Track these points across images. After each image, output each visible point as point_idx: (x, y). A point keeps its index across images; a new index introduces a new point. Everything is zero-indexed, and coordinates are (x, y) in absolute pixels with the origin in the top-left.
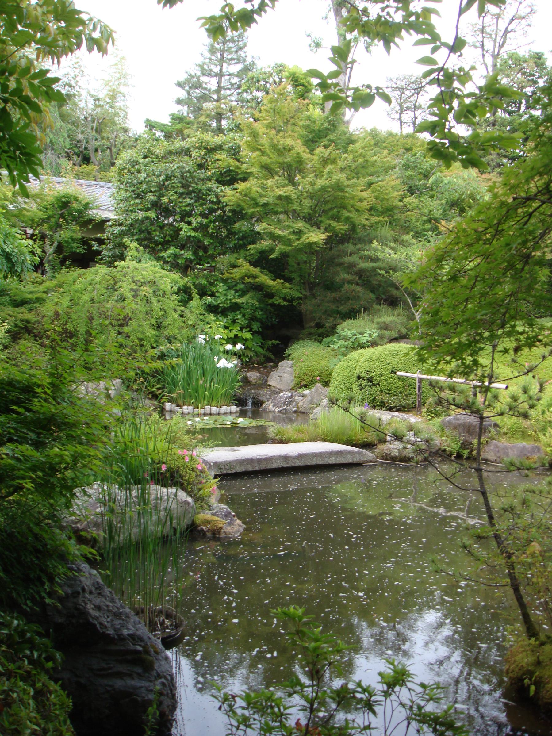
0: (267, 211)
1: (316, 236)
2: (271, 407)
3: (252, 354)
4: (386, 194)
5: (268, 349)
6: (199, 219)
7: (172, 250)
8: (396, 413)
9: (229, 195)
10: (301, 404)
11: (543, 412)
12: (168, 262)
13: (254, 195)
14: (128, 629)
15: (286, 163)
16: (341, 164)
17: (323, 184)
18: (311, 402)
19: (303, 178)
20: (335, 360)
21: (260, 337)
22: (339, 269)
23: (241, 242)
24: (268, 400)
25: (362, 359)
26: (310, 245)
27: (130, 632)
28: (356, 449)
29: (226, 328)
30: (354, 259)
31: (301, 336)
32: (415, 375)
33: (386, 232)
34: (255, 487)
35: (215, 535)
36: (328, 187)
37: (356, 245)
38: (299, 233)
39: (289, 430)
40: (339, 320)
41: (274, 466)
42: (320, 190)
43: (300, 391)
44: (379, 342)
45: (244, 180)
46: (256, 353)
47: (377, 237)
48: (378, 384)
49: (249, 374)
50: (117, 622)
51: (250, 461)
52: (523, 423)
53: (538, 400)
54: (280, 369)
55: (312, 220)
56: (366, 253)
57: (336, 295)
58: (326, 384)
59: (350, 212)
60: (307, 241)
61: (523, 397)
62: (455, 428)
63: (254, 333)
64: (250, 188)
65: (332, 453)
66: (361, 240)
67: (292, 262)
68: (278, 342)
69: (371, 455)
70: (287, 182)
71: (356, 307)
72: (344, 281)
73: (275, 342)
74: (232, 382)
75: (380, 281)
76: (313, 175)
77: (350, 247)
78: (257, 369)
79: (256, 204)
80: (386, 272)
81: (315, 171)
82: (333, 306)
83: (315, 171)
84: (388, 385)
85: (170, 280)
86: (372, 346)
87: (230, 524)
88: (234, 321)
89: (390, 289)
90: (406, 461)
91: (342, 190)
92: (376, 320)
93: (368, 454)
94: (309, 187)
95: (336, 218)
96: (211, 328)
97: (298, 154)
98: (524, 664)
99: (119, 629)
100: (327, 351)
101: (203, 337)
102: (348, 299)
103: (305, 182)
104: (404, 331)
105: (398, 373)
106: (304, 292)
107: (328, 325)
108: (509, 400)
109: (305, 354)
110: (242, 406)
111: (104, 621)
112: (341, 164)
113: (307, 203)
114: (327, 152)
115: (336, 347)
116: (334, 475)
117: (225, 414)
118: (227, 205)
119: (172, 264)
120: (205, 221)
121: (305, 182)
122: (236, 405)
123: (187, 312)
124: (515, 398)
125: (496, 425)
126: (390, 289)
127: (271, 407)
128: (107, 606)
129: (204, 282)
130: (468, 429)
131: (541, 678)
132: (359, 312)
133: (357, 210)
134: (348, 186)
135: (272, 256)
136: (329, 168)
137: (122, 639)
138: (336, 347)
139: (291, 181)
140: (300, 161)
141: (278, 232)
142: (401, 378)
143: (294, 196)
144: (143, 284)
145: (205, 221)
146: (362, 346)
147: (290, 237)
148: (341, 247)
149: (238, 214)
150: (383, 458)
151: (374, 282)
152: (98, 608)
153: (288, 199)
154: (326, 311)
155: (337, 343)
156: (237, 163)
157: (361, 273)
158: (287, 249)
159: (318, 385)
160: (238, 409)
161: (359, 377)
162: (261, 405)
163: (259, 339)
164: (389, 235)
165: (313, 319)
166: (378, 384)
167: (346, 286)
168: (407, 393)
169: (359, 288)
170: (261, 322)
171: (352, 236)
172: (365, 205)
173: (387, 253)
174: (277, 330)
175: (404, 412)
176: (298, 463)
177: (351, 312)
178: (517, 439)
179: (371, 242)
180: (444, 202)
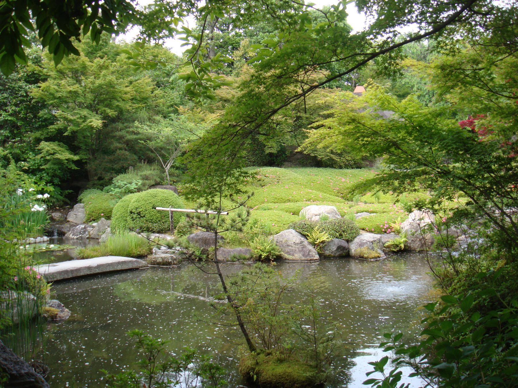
0: (61, 102)
1: (97, 122)
3: (54, 200)
4: (142, 88)
5: (66, 197)
8: (157, 235)
9: (35, 91)
10: (91, 232)
11: (251, 228)
14: (24, 370)
15: (75, 68)
16: (111, 69)
17: (100, 83)
18: (99, 231)
19: (86, 79)
20: (113, 201)
21: (59, 188)
22: (113, 140)
23: (44, 123)
25: (133, 200)
27: (26, 371)
28: (134, 259)
29: (35, 183)
30: (123, 133)
31: (88, 186)
32: (168, 209)
33: (144, 114)
34: (74, 288)
35: (53, 319)
37: (123, 123)
38: (85, 118)
39: (89, 249)
40: (114, 175)
41: (82, 274)
42: (98, 87)
43: (90, 224)
44: (142, 188)
45: (44, 80)
46: (57, 199)
49: (53, 214)
50: (17, 367)
51: (66, 272)
52: (240, 235)
53: (247, 221)
54: (75, 210)
56: (131, 130)
57: (111, 157)
58: (108, 218)
59: (118, 101)
61: (238, 220)
62: (197, 242)
65: (119, 263)
66: (127, 120)
67: (80, 136)
69: (144, 262)
70: (75, 82)
71: (125, 165)
72: (117, 148)
73: (70, 191)
74: (43, 221)
75: (141, 147)
76: (93, 77)
77: (120, 125)
78: (59, 210)
79: (55, 98)
80: (145, 141)
81: (94, 74)
83: (94, 74)
84: (151, 216)
87: (62, 311)
88: (41, 179)
89: (147, 152)
90: (167, 265)
91: (114, 87)
93: (142, 262)
95: (109, 106)
96: (25, 183)
97: (83, 62)
98: (250, 365)
99: (19, 371)
100: (107, 196)
101: (21, 190)
103: (88, 81)
104: (158, 180)
105: (157, 208)
106: (89, 156)
107: (107, 178)
108: (230, 221)
109: (92, 199)
110: (50, 236)
111: (9, 366)
112: (111, 69)
113: (90, 96)
114: (102, 61)
116: (117, 277)
117: (40, 242)
118: (33, 98)
120: (18, 109)
121: (88, 81)
122: (46, 236)
124: (234, 221)
125: (222, 238)
126: (147, 152)
127: (71, 236)
128: (10, 358)
129: (18, 151)
130: (205, 242)
131: (259, 371)
132: (128, 168)
133: (123, 100)
134: (117, 84)
135: (66, 134)
136: (104, 72)
137: (21, 375)
138: (113, 194)
139: (79, 81)
140: (84, 67)
141: (70, 117)
142: (159, 211)
143: (80, 92)
145: (18, 109)
146: (131, 192)
147: (79, 120)
148: (114, 125)
149: (42, 104)
150: (152, 264)
151: (137, 148)
152: (5, 359)
153: (75, 94)
154: (105, 168)
156: (40, 68)
158: (75, 129)
159: (103, 219)
160: (48, 239)
161: (131, 212)
164: (145, 116)
166: (144, 216)
168: (163, 221)
169: (127, 153)
171: (121, 117)
172: (128, 96)
173: (145, 129)
174: (70, 185)
175: (162, 233)
176: (97, 271)
178: (236, 245)
179: (134, 121)
180: (181, 93)
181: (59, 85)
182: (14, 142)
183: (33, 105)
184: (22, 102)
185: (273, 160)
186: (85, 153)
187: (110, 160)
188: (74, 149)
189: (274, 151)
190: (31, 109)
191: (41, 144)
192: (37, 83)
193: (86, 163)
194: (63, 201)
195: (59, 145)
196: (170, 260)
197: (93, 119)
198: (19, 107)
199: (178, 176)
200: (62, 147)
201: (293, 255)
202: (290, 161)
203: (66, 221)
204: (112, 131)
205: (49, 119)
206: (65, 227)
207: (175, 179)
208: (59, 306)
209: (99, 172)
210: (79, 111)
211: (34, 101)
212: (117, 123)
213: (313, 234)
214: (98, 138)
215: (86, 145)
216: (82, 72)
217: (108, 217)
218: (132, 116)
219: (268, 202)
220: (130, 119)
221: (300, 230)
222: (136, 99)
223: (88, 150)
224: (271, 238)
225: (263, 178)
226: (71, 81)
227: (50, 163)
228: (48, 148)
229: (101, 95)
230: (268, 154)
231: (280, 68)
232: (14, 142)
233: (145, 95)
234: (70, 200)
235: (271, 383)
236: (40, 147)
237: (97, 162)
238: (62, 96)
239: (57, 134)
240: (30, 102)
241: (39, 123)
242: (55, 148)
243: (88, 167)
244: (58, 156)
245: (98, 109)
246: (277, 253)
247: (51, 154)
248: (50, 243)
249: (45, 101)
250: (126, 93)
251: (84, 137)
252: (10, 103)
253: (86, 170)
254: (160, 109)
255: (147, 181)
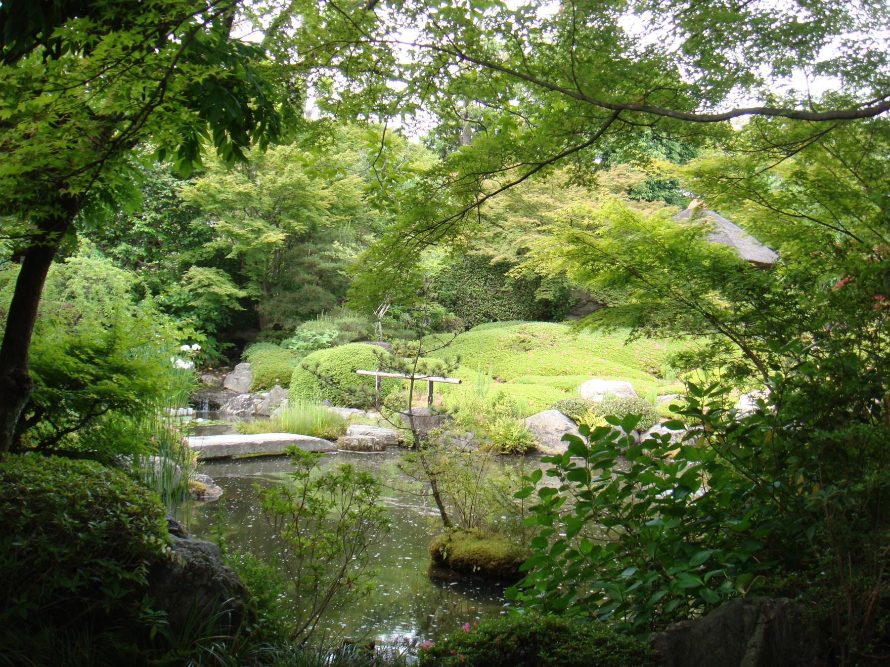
0: (227, 206)
1: (275, 236)
2: (228, 410)
3: (207, 356)
5: (223, 353)
6: (153, 214)
7: (123, 246)
8: (355, 410)
10: (259, 406)
12: (118, 258)
13: (212, 191)
19: (263, 174)
21: (214, 339)
22: (298, 269)
23: (196, 239)
24: (226, 402)
26: (270, 245)
28: (318, 439)
30: (315, 258)
31: (258, 338)
33: (348, 230)
36: (289, 185)
37: (316, 244)
38: (258, 232)
40: (298, 322)
42: (280, 188)
43: (258, 393)
47: (338, 237)
48: (339, 383)
51: (220, 447)
55: (271, 218)
56: (327, 253)
57: (296, 295)
58: (286, 385)
59: (310, 210)
60: (266, 240)
63: (208, 334)
64: (209, 185)
66: (322, 240)
67: (249, 260)
68: (233, 345)
70: (246, 179)
71: (316, 308)
72: (304, 281)
75: (341, 282)
76: (274, 172)
77: (310, 246)
78: (213, 372)
79: (216, 202)
81: (276, 168)
82: (292, 307)
85: (123, 278)
86: (332, 346)
90: (364, 450)
91: (303, 189)
92: (337, 321)
94: (269, 185)
95: (296, 217)
102: (308, 300)
104: (365, 332)
106: (262, 292)
109: (262, 357)
113: (267, 200)
115: (295, 348)
118: (183, 201)
119: (123, 260)
120: (159, 216)
123: (141, 313)
129: (156, 280)
132: (320, 313)
133: (318, 209)
135: (229, 257)
136: (290, 165)
139: (252, 178)
141: (236, 230)
143: (254, 194)
144: (97, 281)
145: (159, 216)
146: (322, 347)
147: (249, 235)
148: (302, 246)
149: (196, 210)
151: (335, 283)
153: (247, 196)
155: (295, 343)
157: (321, 274)
158: (244, 248)
159: (278, 387)
162: (218, 408)
163: (213, 342)
165: (271, 321)
166: (339, 383)
167: (306, 286)
169: (319, 289)
170: (217, 325)
171: (313, 235)
174: (233, 334)
177: (310, 313)
179: (332, 241)
181: (221, 182)
182: (150, 267)
183: (182, 212)
184: (165, 205)
185: (551, 312)
186: (256, 287)
187: (294, 299)
188: (240, 281)
189: (549, 296)
190: (179, 216)
191: (191, 269)
192: (190, 178)
193: (257, 302)
194: (219, 359)
195: (218, 273)
196: (370, 444)
197: (271, 233)
198: (161, 213)
199: (396, 329)
200: (222, 276)
201: (553, 447)
202: (577, 315)
203: (221, 387)
204: (299, 255)
205: (205, 233)
206: (220, 397)
207: (391, 333)
208: (208, 482)
209: (276, 316)
210: (250, 222)
211: (184, 204)
212: (307, 244)
213: (586, 418)
214: (277, 266)
215: (258, 275)
216: (257, 164)
217: (286, 384)
218: (330, 234)
219: (531, 373)
220: (327, 238)
221: (568, 412)
222: (337, 209)
223: (261, 283)
224: (521, 422)
225: (529, 337)
226: (241, 177)
227: (203, 298)
228: (201, 277)
229: (284, 199)
230: (540, 301)
231: (45, 212)
232: (150, 267)
233: (351, 203)
234: (230, 358)
235: (462, 560)
236: (189, 274)
237: (272, 302)
238: (227, 199)
239: (216, 256)
240: (177, 206)
241: (189, 239)
242: (213, 276)
243: (260, 308)
244: (215, 289)
245: (280, 221)
246: (528, 442)
247: (205, 286)
248: (197, 418)
249: (200, 206)
250: (322, 199)
251: (256, 263)
252: (148, 206)
253: (257, 313)
254: (374, 225)
255: (347, 333)
